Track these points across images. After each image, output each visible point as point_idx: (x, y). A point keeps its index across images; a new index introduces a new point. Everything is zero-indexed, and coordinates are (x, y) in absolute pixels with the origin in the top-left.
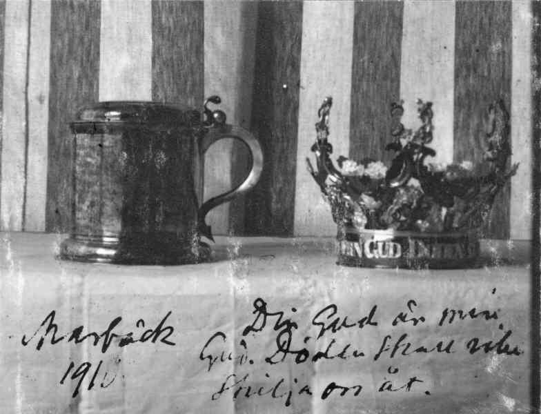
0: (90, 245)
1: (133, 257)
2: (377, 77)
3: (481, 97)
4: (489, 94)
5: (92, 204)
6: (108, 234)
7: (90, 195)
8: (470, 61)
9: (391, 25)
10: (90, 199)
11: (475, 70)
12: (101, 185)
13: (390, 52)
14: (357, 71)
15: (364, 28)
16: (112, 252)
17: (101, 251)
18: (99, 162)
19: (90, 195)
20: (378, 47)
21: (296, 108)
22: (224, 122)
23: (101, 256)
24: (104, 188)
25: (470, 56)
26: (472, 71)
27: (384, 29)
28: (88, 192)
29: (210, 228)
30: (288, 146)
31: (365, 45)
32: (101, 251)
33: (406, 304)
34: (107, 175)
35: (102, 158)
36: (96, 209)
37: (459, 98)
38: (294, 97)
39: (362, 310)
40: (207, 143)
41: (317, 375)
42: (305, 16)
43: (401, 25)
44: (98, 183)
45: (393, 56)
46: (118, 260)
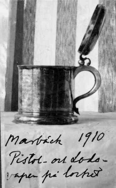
0: (28, 117)
1: (47, 121)
2: (66, 44)
3: (109, 53)
4: (113, 52)
5: (29, 99)
6: (36, 112)
7: (28, 95)
8: (105, 38)
9: (72, 23)
10: (28, 97)
11: (107, 42)
12: (33, 91)
13: (71, 34)
14: (58, 42)
15: (61, 24)
16: (37, 119)
17: (33, 119)
18: (32, 82)
19: (28, 95)
20: (67, 32)
21: (33, 58)
22: (84, 64)
23: (33, 121)
24: (34, 92)
25: (105, 36)
26: (105, 42)
27: (69, 25)
28: (27, 94)
29: (77, 109)
30: (106, 75)
31: (61, 32)
32: (33, 119)
33: (98, 141)
34: (35, 86)
35: (33, 79)
36: (31, 101)
37: (100, 54)
38: (31, 53)
39: (46, 145)
40: (76, 74)
41: (41, 173)
42: (36, 20)
43: (76, 23)
44: (31, 90)
45: (73, 35)
46: (40, 123)
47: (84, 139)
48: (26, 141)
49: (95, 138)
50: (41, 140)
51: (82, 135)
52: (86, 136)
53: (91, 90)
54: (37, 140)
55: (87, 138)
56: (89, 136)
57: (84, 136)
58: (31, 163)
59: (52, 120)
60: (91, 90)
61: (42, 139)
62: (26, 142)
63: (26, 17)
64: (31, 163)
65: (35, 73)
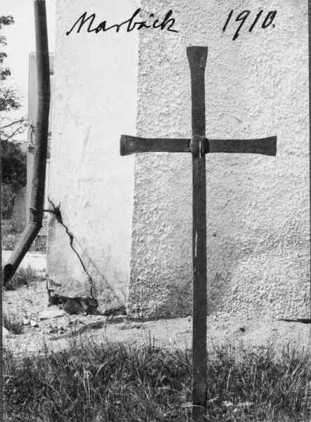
32: (152, 342)
47: (233, 26)
48: (105, 26)
49: (256, 25)
50: (136, 23)
51: (230, 15)
52: (237, 20)
53: (81, 26)
54: (128, 23)
55: (240, 22)
56: (245, 18)
57: (234, 17)
58: (160, 27)
59: (80, 348)
60: (81, 26)
61: (136, 21)
62: (106, 28)
63: (260, 112)
64: (160, 27)
65: (161, 183)
